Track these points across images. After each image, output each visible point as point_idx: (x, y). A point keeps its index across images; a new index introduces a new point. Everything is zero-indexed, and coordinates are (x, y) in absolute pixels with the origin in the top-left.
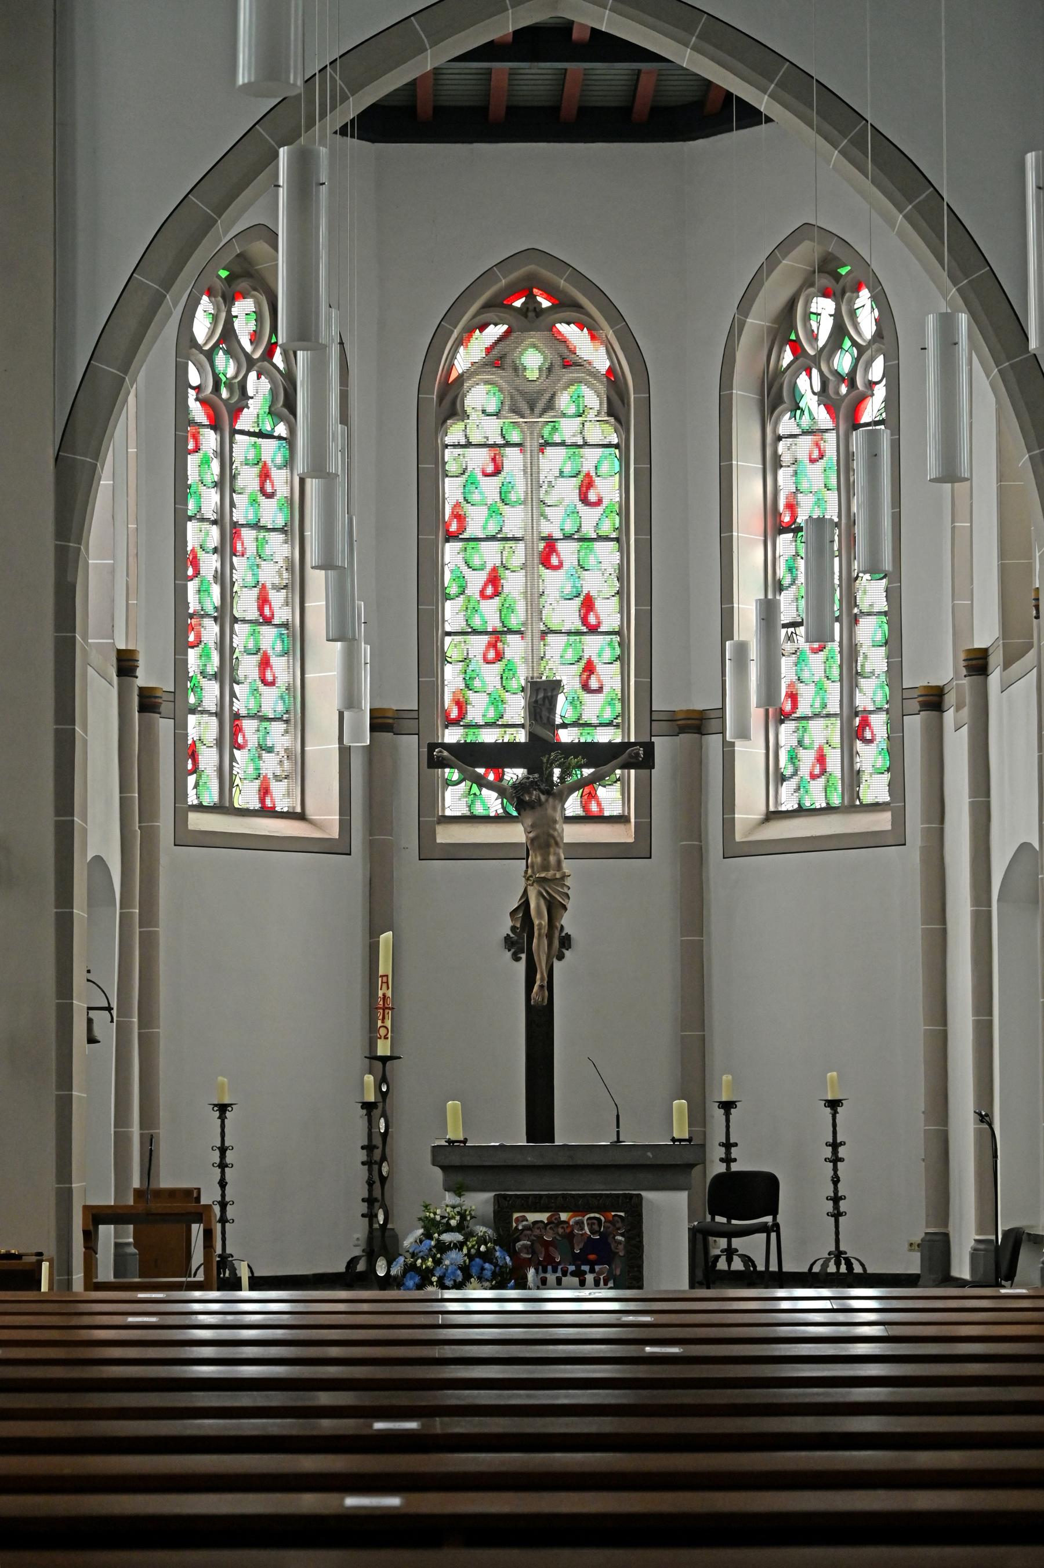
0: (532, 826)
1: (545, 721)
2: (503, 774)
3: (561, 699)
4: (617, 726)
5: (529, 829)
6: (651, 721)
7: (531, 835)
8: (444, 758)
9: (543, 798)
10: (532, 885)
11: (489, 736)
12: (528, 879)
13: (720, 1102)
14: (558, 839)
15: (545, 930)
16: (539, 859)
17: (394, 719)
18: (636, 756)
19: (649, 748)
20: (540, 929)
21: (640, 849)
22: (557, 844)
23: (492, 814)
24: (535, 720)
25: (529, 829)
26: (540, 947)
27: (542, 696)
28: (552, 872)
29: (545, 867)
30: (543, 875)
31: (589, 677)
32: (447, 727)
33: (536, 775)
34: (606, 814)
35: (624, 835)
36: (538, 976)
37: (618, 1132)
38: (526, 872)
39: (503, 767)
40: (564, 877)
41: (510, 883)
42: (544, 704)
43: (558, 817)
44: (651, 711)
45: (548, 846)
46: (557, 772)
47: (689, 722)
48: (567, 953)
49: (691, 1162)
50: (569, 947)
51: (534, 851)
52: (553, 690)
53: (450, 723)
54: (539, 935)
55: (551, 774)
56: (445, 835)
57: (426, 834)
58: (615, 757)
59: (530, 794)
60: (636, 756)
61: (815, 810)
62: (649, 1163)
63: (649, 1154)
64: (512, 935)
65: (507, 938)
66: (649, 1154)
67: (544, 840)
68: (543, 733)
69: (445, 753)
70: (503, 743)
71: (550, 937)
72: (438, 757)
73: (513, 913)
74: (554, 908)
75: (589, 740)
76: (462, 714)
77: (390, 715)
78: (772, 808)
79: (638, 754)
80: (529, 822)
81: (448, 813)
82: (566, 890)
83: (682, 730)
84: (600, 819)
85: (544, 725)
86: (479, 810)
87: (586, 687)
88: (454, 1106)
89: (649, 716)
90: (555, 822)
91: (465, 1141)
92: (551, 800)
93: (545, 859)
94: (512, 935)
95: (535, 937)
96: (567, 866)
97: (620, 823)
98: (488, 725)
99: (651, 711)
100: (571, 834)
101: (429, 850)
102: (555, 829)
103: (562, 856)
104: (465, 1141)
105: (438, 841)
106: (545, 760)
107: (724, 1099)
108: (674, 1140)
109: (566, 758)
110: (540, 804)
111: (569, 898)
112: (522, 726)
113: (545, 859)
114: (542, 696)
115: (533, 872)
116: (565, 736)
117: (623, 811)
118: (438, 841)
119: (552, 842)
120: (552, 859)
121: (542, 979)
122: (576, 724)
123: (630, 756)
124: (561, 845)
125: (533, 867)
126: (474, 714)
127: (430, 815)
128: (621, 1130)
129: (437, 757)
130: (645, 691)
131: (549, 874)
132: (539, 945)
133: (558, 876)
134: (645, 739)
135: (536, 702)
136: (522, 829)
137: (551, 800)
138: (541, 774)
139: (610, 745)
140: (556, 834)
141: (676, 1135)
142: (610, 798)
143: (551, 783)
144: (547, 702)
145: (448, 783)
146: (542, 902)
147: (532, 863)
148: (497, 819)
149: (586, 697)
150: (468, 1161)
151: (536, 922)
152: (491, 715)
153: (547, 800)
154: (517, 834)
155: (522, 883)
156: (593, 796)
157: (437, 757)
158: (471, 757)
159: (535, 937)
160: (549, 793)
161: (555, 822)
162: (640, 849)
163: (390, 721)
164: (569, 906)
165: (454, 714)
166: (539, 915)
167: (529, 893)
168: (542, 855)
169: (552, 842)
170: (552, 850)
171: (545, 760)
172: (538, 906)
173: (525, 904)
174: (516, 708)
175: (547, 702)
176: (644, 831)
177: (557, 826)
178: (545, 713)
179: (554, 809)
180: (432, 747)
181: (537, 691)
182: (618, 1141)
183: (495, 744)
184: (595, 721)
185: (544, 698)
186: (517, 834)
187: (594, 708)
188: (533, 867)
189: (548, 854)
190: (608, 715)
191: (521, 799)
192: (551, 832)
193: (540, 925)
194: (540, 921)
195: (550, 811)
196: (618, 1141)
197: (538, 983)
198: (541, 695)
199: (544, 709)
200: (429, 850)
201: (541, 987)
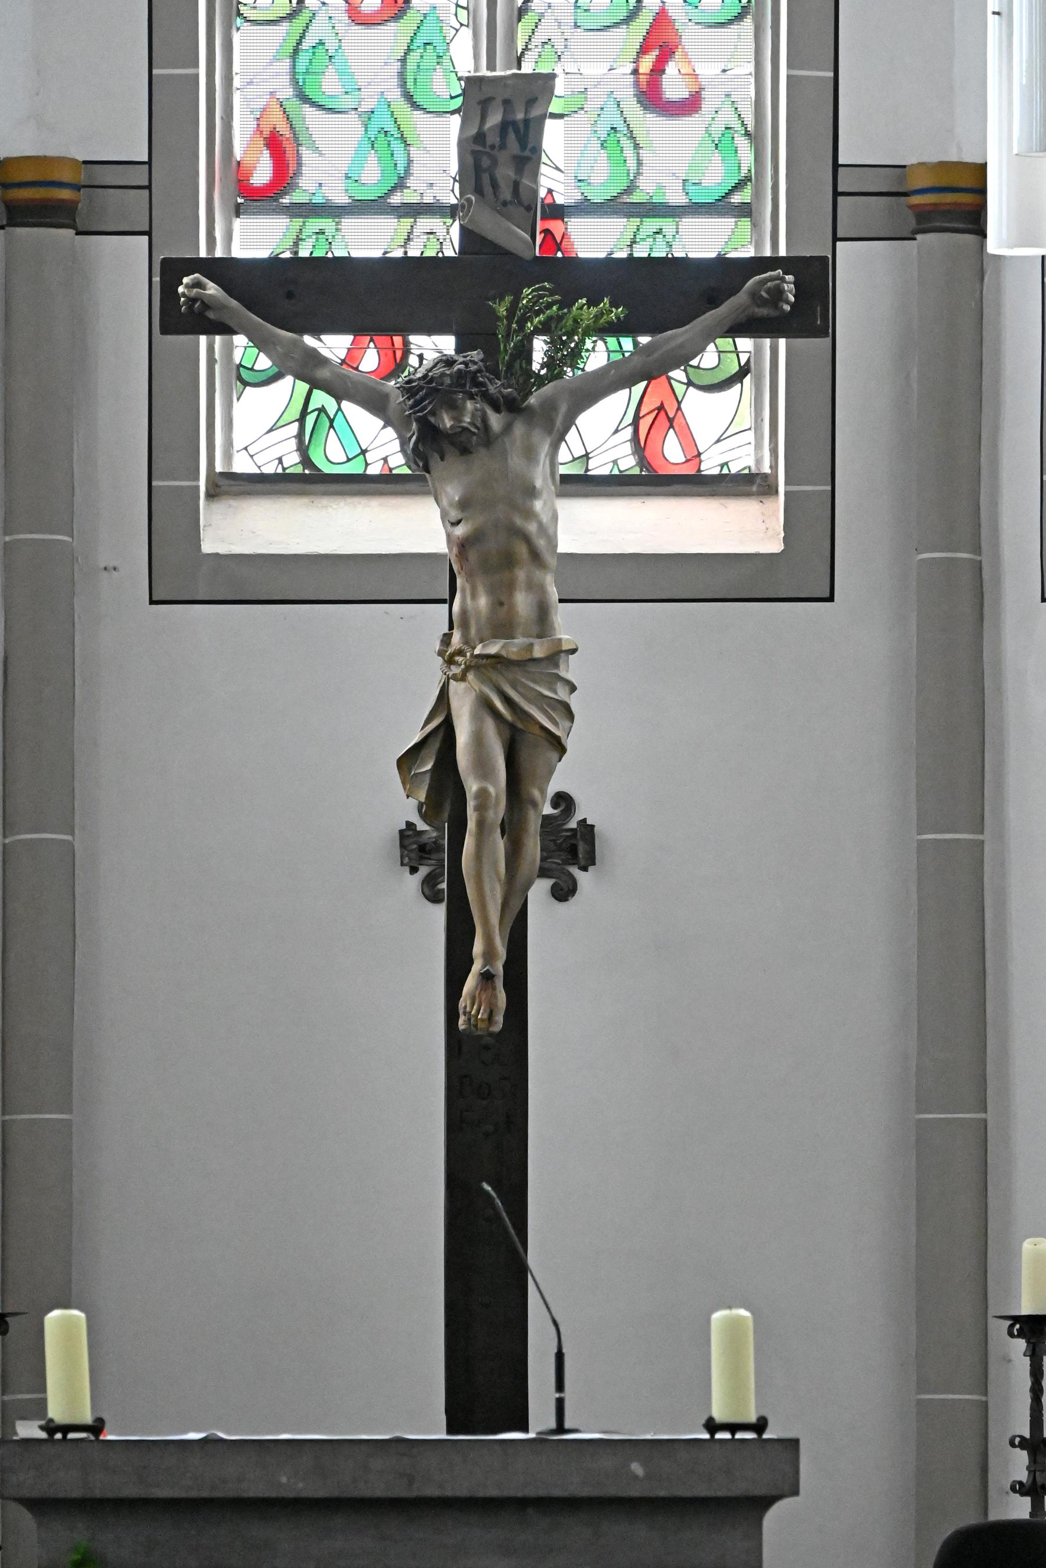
0: (464, 504)
1: (506, 194)
2: (406, 352)
3: (554, 138)
4: (745, 211)
5: (454, 515)
6: (836, 194)
7: (460, 531)
8: (206, 305)
9: (496, 421)
10: (462, 678)
11: (367, 240)
12: (450, 661)
13: (1016, 1319)
14: (541, 543)
15: (498, 811)
16: (483, 602)
17: (77, 187)
18: (792, 301)
19: (814, 277)
20: (481, 808)
21: (798, 575)
22: (535, 556)
23: (374, 470)
24: (479, 191)
25: (454, 515)
26: (483, 858)
27: (504, 122)
28: (520, 641)
29: (502, 626)
30: (493, 649)
31: (658, 69)
32: (238, 211)
33: (476, 355)
34: (710, 467)
35: (750, 529)
36: (478, 948)
37: (560, 1404)
38: (446, 639)
39: (406, 330)
40: (557, 655)
41: (397, 673)
42: (503, 146)
43: (540, 478)
44: (836, 166)
45: (509, 561)
46: (540, 347)
47: (949, 198)
48: (584, 879)
49: (759, 1491)
50: (589, 862)
51: (470, 576)
52: (531, 102)
53: (252, 199)
54: (481, 824)
55: (525, 352)
56: (236, 530)
57: (169, 523)
58: (713, 300)
59: (455, 408)
60: (792, 301)
61: (362, 479)
62: (634, 1492)
63: (637, 1468)
64: (422, 826)
65: (408, 833)
66: (637, 1468)
67: (499, 549)
68: (511, 235)
69: (212, 289)
70: (406, 260)
71: (512, 828)
72: (192, 300)
73: (407, 761)
74: (527, 745)
75: (659, 253)
76: (284, 175)
77: (66, 176)
78: (219, 468)
79: (778, 294)
80: (453, 492)
81: (242, 465)
82: (562, 694)
83: (927, 221)
84: (694, 483)
85: (502, 208)
86: (332, 455)
87: (651, 96)
88: (68, 1325)
89: (836, 187)
90: (532, 492)
91: (97, 1427)
92: (519, 429)
93: (501, 601)
94: (422, 826)
95: (491, 827)
96: (568, 623)
97: (748, 495)
98: (360, 208)
99: (836, 166)
100: (585, 528)
101: (182, 576)
102: (530, 514)
103: (554, 594)
104: (97, 1427)
105: (208, 547)
106: (502, 311)
107: (1026, 1310)
108: (712, 1426)
109: (567, 303)
110: (487, 438)
111: (570, 716)
112: (452, 211)
113: (501, 601)
114: (504, 122)
115: (466, 640)
116: (592, 240)
117: (759, 461)
118: (208, 547)
119: (522, 550)
120: (523, 602)
121: (489, 955)
122: (617, 206)
123: (754, 295)
124: (552, 562)
125: (465, 625)
126: (319, 177)
127: (176, 472)
128: (568, 1395)
129: (191, 301)
130: (819, 106)
131: (512, 648)
132: (478, 856)
133: (538, 652)
134: (818, 249)
135: (480, 138)
136: (437, 512)
137: (519, 429)
138: (491, 352)
139: (722, 263)
140: (532, 528)
141: (719, 1414)
142: (724, 421)
143: (529, 381)
144: (512, 136)
145: (242, 378)
146: (490, 727)
147: (464, 612)
148: (386, 484)
149: (651, 126)
150: (102, 1485)
151: (472, 786)
152: (373, 179)
153: (508, 428)
154: (417, 527)
155: (434, 671)
156: (668, 416)
157: (191, 301)
158: (292, 298)
159: (491, 827)
160: (512, 407)
161: (532, 492)
162: (798, 575)
163: (65, 194)
164: (570, 743)
165: (262, 174)
166: (482, 766)
167: (455, 703)
168: (492, 591)
169: (522, 550)
170: (521, 575)
171: (502, 311)
172: (478, 740)
173: (442, 735)
174: (437, 162)
175: (512, 136)
176: (814, 523)
177: (538, 505)
178: (505, 172)
179: (530, 454)
180: (172, 271)
181: (485, 105)
182: (561, 1429)
183: (385, 263)
184: (676, 197)
185: (504, 126)
186: (417, 527)
187: (679, 158)
188: (465, 625)
189: (511, 587)
190: (715, 179)
191: (439, 431)
192: (519, 521)
193: (482, 795)
194: (483, 784)
195: (515, 461)
196: (561, 1429)
197: (477, 967)
198: (495, 119)
199: (503, 156)
200: (182, 576)
201: (487, 977)
